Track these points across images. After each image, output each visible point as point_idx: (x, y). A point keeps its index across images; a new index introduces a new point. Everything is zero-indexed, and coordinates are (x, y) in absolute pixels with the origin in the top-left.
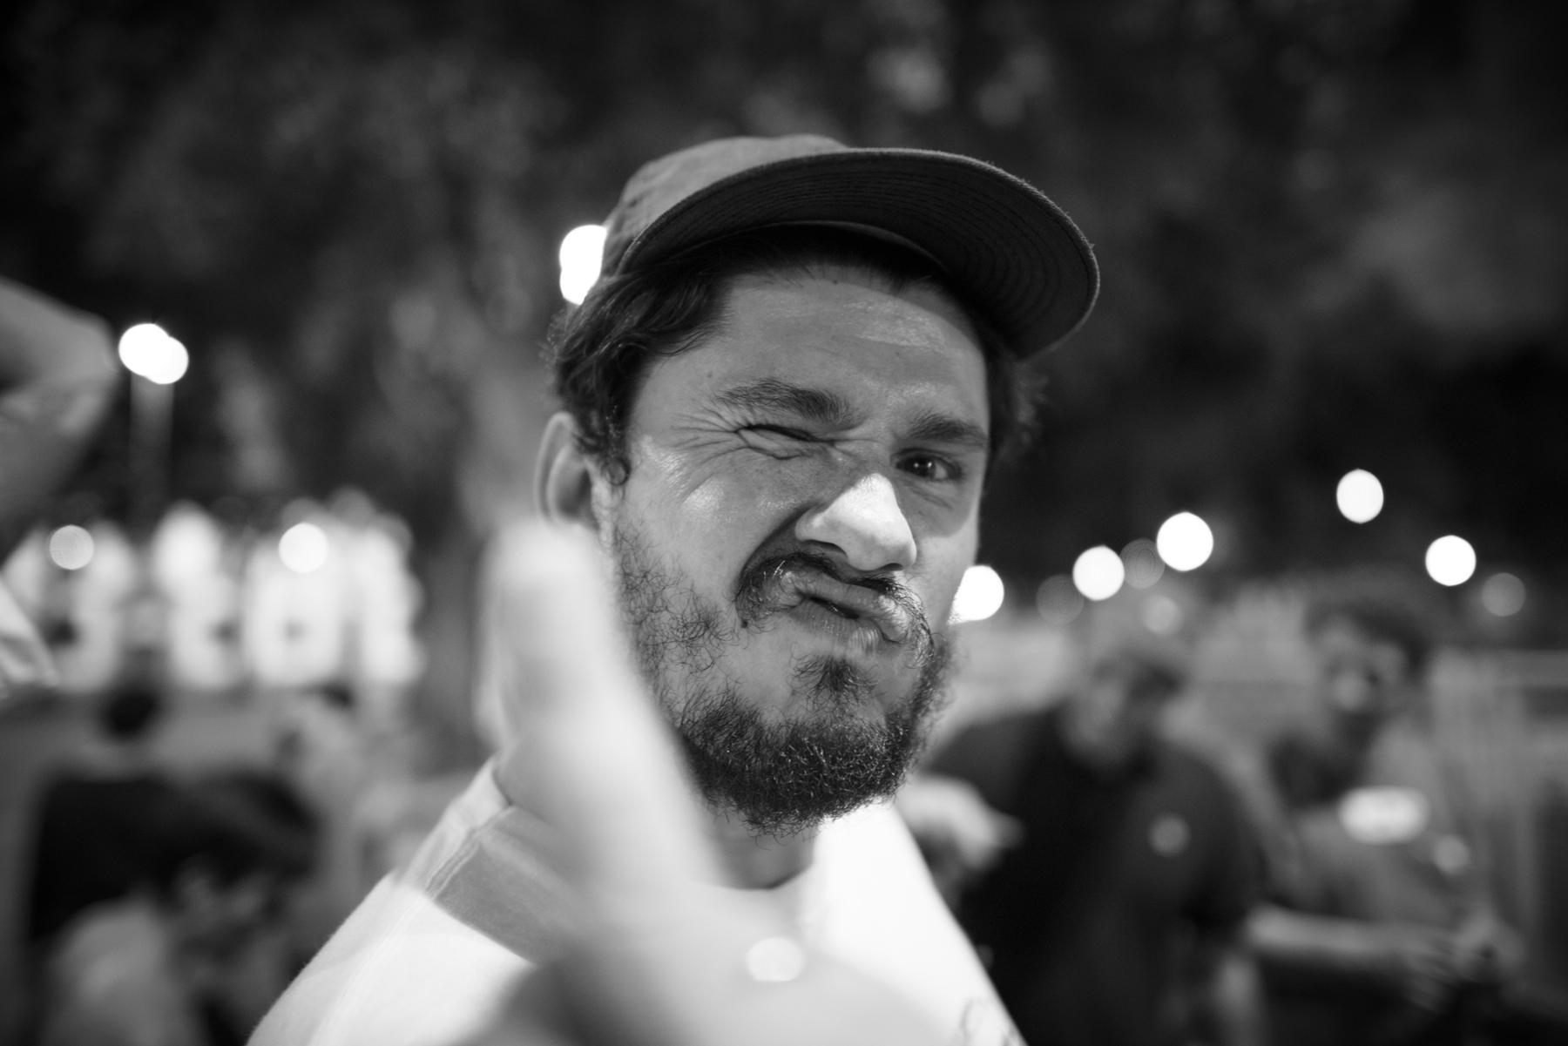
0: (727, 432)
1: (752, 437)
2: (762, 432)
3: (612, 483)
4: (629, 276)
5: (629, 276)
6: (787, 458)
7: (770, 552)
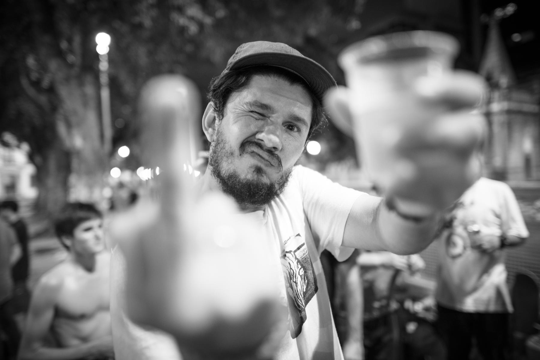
0: (246, 111)
1: (251, 114)
2: (253, 113)
3: (219, 119)
4: (231, 71)
5: (231, 71)
6: (259, 120)
7: (249, 139)
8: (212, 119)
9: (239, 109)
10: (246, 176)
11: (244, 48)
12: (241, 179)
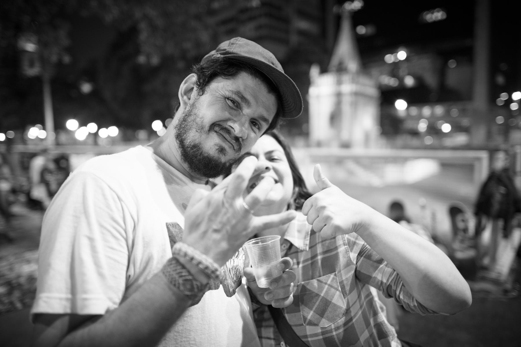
8: (189, 88)
9: (220, 94)
10: (203, 65)
11: (239, 42)
12: (204, 152)
